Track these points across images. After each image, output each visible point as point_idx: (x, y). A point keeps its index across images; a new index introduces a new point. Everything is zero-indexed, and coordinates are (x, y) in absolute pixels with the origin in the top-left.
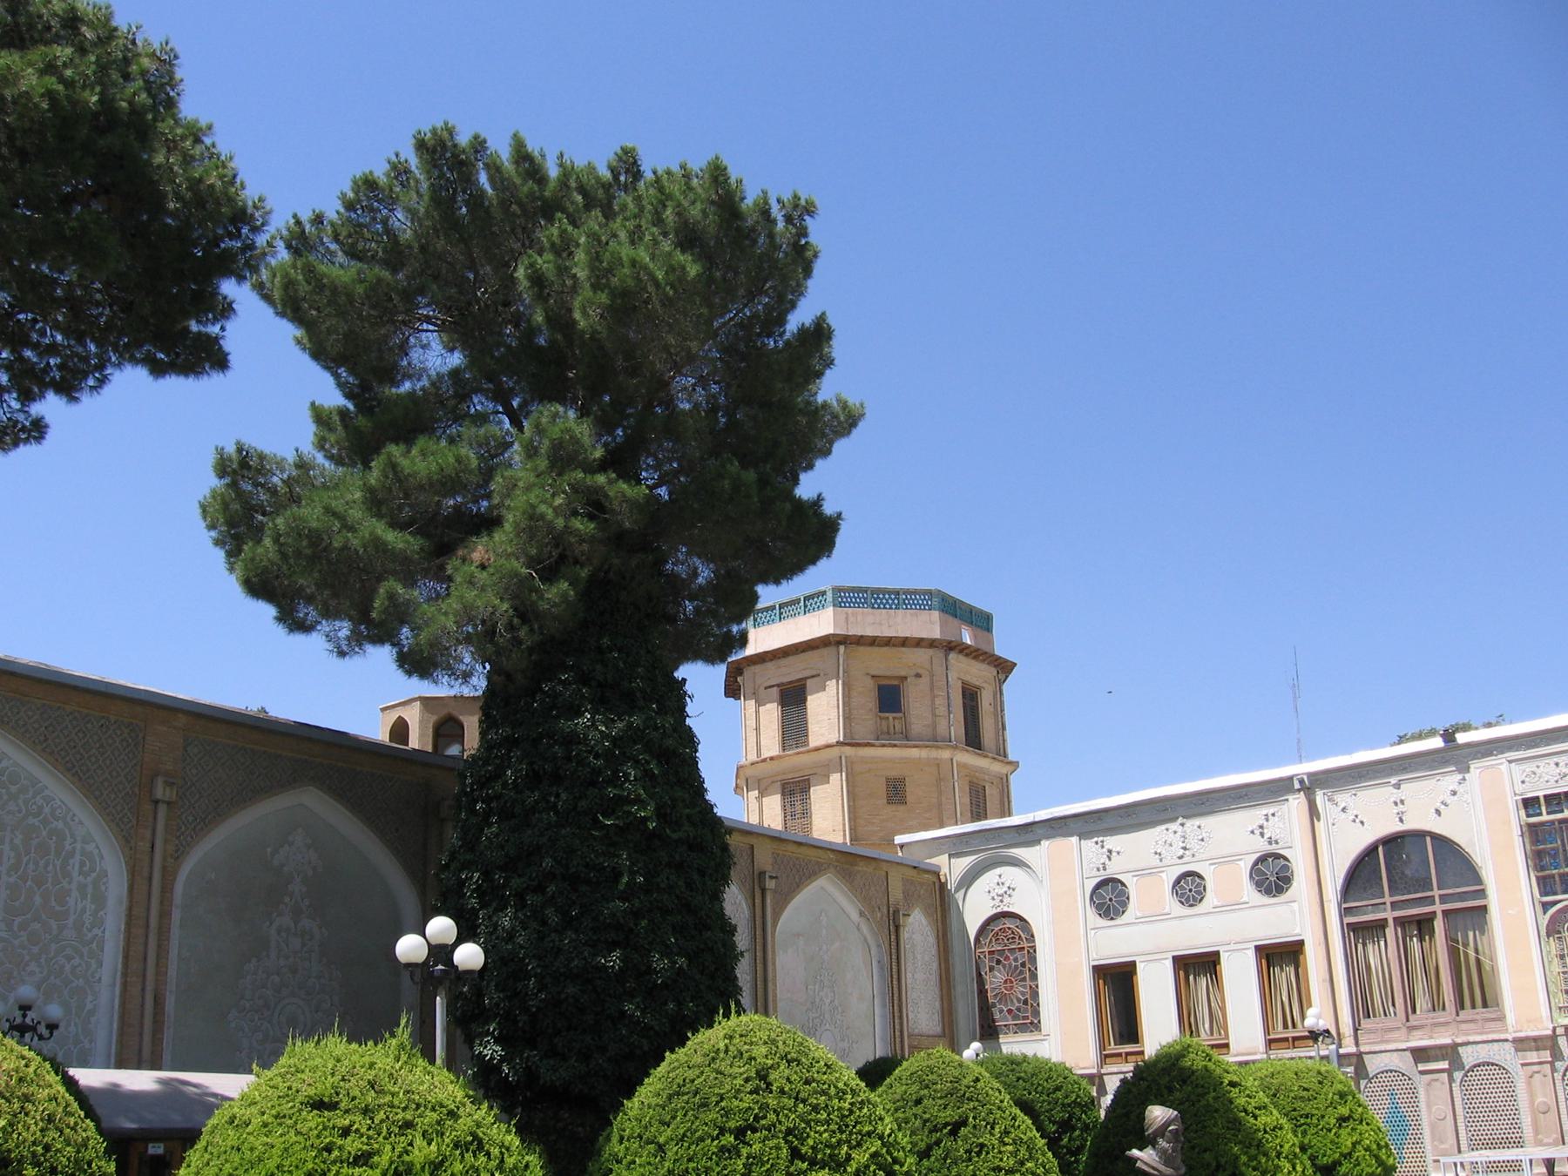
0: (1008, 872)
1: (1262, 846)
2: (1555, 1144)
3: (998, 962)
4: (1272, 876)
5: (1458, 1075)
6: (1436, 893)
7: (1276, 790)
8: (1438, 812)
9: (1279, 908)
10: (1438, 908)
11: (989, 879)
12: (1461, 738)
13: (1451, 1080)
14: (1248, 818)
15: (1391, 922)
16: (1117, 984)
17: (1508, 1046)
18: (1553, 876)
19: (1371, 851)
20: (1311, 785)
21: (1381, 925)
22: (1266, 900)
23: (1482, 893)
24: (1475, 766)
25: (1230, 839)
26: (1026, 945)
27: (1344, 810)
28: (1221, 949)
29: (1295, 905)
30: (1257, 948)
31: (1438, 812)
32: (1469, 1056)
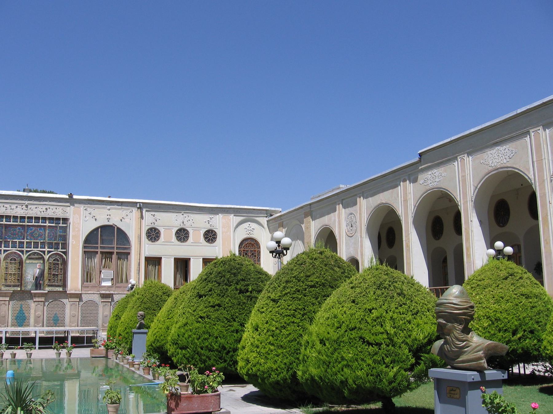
0: (253, 225)
1: (208, 227)
2: (40, 327)
3: (246, 254)
4: (182, 235)
5: (47, 304)
6: (99, 245)
7: (134, 204)
8: (121, 220)
9: (183, 247)
10: (115, 251)
11: (246, 225)
12: (75, 197)
13: (44, 305)
14: (205, 217)
15: (99, 253)
16: (154, 262)
17: (98, 296)
18: (52, 243)
19: (97, 229)
20: (141, 207)
21: (112, 253)
22: (179, 243)
23: (129, 248)
24: (76, 205)
25: (198, 224)
26: (257, 250)
27: (90, 214)
28: (191, 258)
29: (217, 248)
30: (175, 258)
31: (121, 220)
32: (85, 298)
